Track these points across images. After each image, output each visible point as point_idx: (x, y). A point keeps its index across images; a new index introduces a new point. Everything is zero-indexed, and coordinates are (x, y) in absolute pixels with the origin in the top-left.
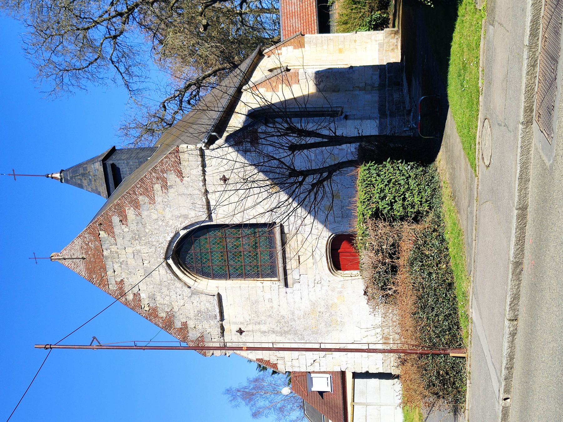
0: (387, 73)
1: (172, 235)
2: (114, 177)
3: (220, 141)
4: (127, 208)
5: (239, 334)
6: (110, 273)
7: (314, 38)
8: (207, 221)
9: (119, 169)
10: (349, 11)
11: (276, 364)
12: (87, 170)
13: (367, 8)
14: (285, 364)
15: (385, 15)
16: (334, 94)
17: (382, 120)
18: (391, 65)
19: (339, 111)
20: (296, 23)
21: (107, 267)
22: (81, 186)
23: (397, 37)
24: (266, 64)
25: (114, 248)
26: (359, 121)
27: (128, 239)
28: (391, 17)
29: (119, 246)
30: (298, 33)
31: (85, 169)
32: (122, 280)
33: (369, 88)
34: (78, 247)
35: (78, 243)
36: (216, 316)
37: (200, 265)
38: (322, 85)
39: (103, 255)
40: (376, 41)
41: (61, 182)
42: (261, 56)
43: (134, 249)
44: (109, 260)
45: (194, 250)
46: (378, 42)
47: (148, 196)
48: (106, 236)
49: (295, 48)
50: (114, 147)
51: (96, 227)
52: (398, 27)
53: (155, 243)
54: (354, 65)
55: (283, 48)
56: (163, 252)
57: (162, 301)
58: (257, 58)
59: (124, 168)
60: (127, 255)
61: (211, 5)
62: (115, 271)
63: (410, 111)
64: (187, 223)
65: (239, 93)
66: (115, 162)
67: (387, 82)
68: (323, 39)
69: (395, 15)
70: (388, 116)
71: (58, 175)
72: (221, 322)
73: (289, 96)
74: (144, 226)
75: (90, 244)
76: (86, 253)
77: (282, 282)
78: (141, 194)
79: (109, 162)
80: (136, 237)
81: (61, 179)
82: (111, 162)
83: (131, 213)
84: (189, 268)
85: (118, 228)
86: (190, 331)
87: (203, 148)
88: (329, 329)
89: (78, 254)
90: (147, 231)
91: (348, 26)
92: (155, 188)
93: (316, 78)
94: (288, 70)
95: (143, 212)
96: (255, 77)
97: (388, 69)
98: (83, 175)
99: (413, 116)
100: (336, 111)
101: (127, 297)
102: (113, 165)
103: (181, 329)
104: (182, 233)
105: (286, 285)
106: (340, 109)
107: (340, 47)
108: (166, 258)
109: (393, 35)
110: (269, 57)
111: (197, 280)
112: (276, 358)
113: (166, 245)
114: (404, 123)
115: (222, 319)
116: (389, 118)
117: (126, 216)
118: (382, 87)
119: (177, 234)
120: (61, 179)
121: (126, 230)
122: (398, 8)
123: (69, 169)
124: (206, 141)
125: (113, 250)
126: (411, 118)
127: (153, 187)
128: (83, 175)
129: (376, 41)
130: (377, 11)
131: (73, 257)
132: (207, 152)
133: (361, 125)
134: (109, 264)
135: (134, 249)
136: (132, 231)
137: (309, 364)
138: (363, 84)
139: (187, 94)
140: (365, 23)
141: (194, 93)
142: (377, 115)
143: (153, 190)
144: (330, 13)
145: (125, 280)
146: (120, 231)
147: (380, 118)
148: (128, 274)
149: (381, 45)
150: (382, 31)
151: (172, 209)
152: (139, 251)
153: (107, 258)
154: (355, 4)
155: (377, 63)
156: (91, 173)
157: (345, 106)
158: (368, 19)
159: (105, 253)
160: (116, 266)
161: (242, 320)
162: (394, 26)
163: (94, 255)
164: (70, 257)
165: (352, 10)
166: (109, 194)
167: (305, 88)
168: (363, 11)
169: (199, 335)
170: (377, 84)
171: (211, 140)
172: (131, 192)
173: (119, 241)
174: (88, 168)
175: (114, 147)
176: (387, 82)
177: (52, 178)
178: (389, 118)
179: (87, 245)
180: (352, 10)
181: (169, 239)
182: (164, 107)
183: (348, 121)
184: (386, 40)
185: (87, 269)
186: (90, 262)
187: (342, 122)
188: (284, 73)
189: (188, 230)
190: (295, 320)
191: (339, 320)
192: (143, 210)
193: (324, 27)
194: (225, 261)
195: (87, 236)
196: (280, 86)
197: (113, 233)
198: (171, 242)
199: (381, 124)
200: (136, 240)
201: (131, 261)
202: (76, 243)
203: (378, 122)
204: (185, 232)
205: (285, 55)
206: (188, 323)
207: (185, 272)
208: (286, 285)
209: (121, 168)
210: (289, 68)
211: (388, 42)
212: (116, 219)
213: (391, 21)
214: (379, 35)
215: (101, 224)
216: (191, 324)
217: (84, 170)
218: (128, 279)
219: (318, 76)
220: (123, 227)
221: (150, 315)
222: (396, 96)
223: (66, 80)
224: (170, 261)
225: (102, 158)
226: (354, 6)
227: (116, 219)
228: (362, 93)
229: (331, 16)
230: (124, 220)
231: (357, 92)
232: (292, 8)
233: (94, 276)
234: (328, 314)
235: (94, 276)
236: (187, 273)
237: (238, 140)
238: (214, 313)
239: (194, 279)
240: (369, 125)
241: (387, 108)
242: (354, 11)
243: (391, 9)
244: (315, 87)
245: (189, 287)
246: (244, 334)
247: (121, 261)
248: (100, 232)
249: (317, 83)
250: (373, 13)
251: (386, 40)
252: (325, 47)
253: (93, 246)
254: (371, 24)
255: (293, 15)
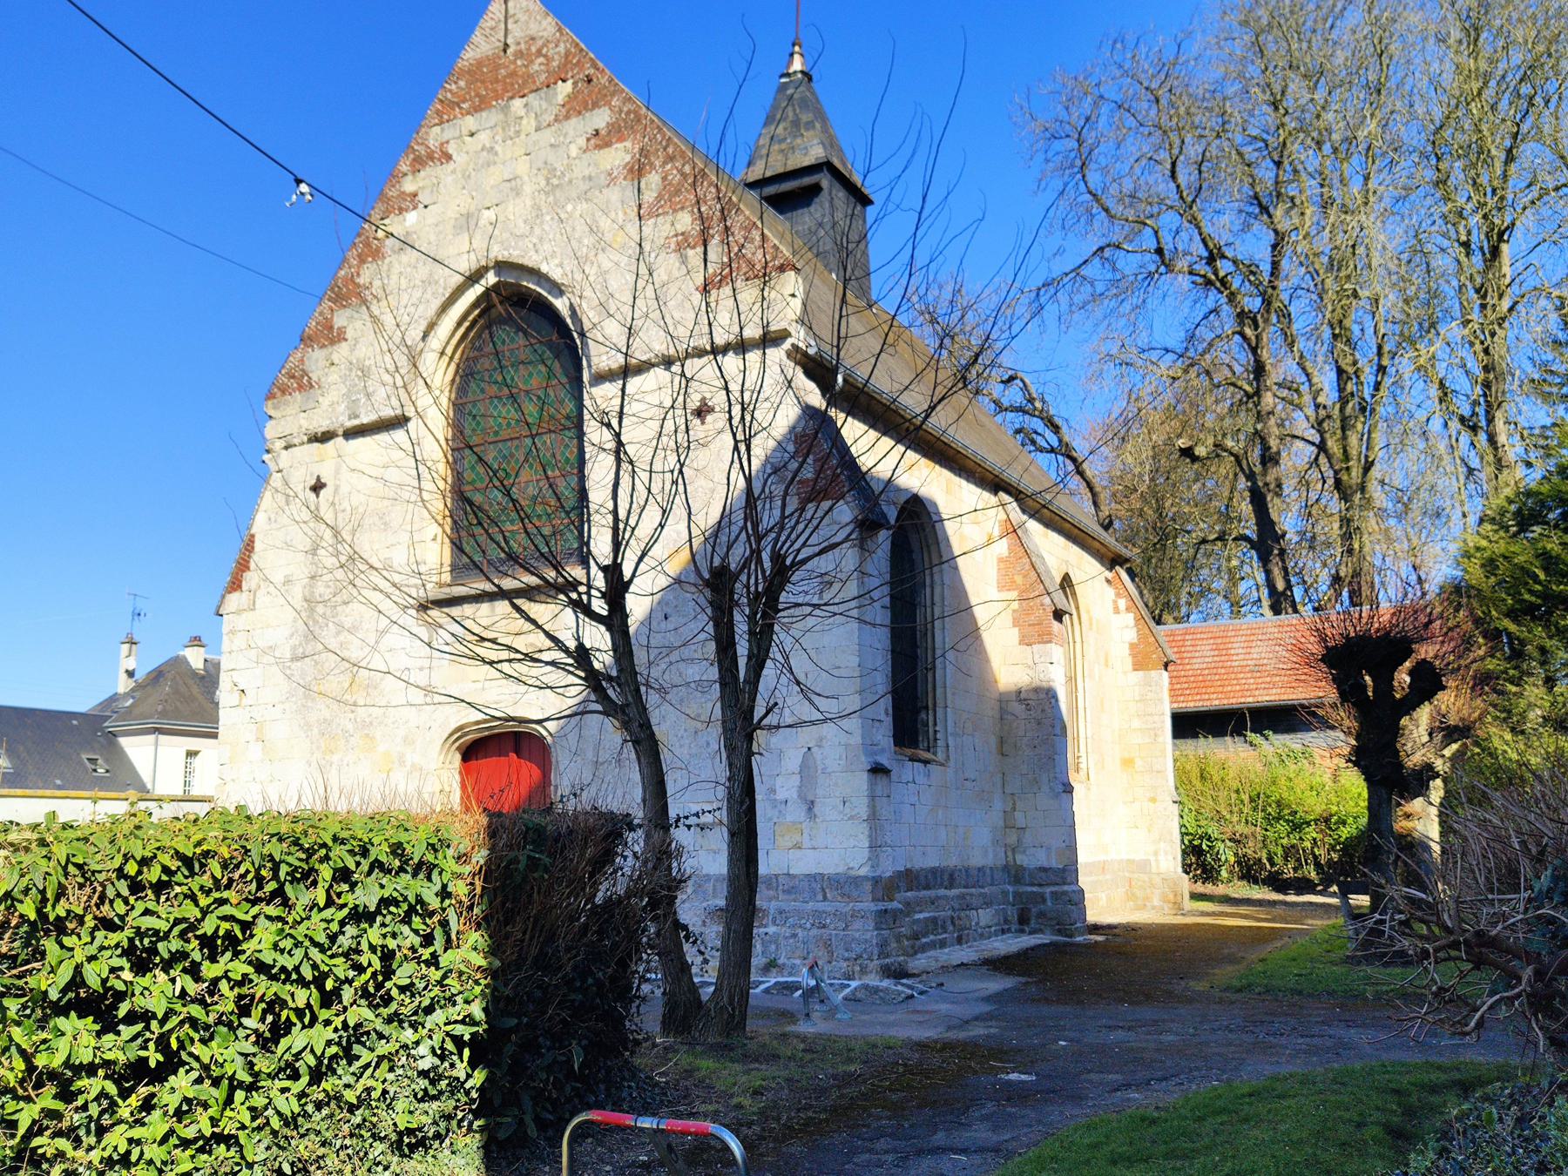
0: (1056, 888)
1: (556, 274)
2: (788, 194)
3: (816, 398)
4: (628, 144)
5: (313, 482)
6: (470, 122)
7: (1158, 699)
8: (590, 366)
9: (809, 205)
10: (1235, 785)
11: (240, 587)
12: (807, 129)
13: (1241, 829)
14: (239, 612)
15: (1224, 874)
16: (993, 740)
17: (868, 886)
18: (1077, 900)
19: (935, 754)
20: (1202, 656)
21: (484, 114)
22: (769, 120)
23: (1167, 908)
24: (1085, 567)
25: (529, 124)
26: (863, 810)
27: (551, 159)
28: (1221, 889)
29: (535, 136)
30: (1169, 652)
31: (810, 125)
32: (449, 157)
33: (1012, 839)
34: (534, 29)
35: (546, 26)
36: (357, 417)
37: (487, 366)
38: (1018, 708)
39: (512, 98)
40: (1156, 853)
41: (783, 76)
42: (1113, 561)
43: (526, 178)
44: (501, 116)
45: (513, 342)
46: (1152, 858)
47: (659, 197)
48: (560, 99)
49: (1132, 646)
50: (870, 202)
51: (581, 70)
52: (1192, 913)
53: (537, 231)
54: (1078, 794)
55: (1131, 616)
56: (515, 255)
57: (396, 269)
58: (1103, 550)
59: (807, 217)
60: (515, 160)
61: (1242, 469)
62: (472, 135)
63: (899, 974)
64: (589, 315)
65: (995, 484)
66: (825, 193)
67: (1029, 889)
68: (1156, 718)
69: (1227, 900)
70: (881, 906)
71: (797, 65)
72: (340, 432)
73: (981, 614)
74: (584, 196)
75: (541, 60)
76: (519, 54)
77: (434, 593)
78: (664, 179)
79: (825, 180)
80: (553, 182)
81: (788, 75)
82: (825, 183)
83: (619, 155)
84: (479, 335)
85: (579, 128)
86: (325, 352)
87: (789, 341)
88: (316, 731)
89: (516, 32)
90: (569, 207)
91: (1192, 785)
92: (680, 215)
93: (1037, 690)
94: (1058, 615)
95: (617, 189)
96: (1046, 536)
97: (1065, 893)
98: (796, 123)
99: (876, 990)
100: (935, 746)
101: (410, 177)
102: (816, 189)
103: (331, 327)
104: (561, 304)
105: (423, 607)
106: (940, 756)
107: (1139, 763)
108: (501, 266)
109: (1171, 896)
110: (1108, 581)
111: (446, 359)
112: (253, 587)
113: (530, 260)
114: (859, 957)
115: (350, 434)
116: (873, 907)
117: (608, 144)
118: (1016, 874)
119: (558, 289)
120: (788, 75)
121: (574, 151)
122: (1243, 910)
123: (813, 93)
124: (811, 351)
125: (524, 122)
126: (873, 980)
127: (682, 208)
128: (796, 123)
129: (1156, 853)
130: (1236, 854)
131: (510, 21)
132: (776, 355)
133: (851, 818)
134: (490, 117)
135: (526, 178)
136: (569, 167)
137: (236, 677)
138: (1021, 822)
139: (1037, 424)
140: (1203, 823)
141: (1039, 439)
142: (888, 869)
143: (675, 211)
144: (1228, 738)
145: (451, 165)
146: (571, 133)
147: (876, 881)
148: (464, 172)
149: (1143, 866)
150: (1180, 870)
151: (620, 259)
152: (517, 192)
153: (505, 110)
154: (1252, 800)
155: (1083, 857)
156: (799, 141)
157: (950, 771)
158: (1213, 830)
159: (517, 103)
160: (484, 138)
161: (344, 489)
162: (1195, 896)
163: (513, 74)
164: (511, 12)
165: (1237, 792)
166: (752, 185)
167: (1008, 658)
168: (1235, 819)
169: (314, 377)
170: (1022, 859)
171: (818, 369)
172: (670, 150)
173: (548, 136)
174: (811, 133)
175: (870, 202)
176: (1029, 889)
177: (792, 55)
178: (873, 907)
179: (539, 53)
180: (1237, 792)
181: (544, 269)
182: (1012, 379)
183: (865, 775)
184: (1157, 880)
185: (480, 63)
186: (497, 67)
187: (863, 758)
188: (1057, 608)
189: (569, 321)
190: (338, 633)
191: (335, 758)
192: (624, 189)
193: (1187, 725)
194: (496, 433)
195: (562, 48)
196: (1014, 595)
197: (567, 117)
198: (534, 273)
199: (856, 881)
200: (548, 180)
201: (495, 175)
202: (544, 23)
203: (863, 872)
204: (565, 312)
205: (1106, 605)
206: (344, 344)
207: (467, 324)
208: (423, 607)
209: (812, 209)
210: (1066, 618)
211: (1152, 886)
212: (601, 118)
213: (1209, 888)
214: (1170, 860)
215: (589, 81)
216: (341, 352)
217: (808, 123)
218: (454, 172)
219: (1042, 696)
220: (582, 142)
221: (367, 244)
222: (985, 917)
223: (1058, 145)
224: (491, 278)
225: (836, 162)
226: (1246, 798)
227: (601, 118)
228: (996, 817)
229: (1219, 740)
230: (600, 140)
231: (998, 805)
232: (1237, 648)
233: (462, 83)
234: (350, 726)
235: (462, 83)
236: (462, 330)
237: (815, 434)
238: (363, 411)
239: (449, 351)
240: (852, 842)
241: (942, 892)
242: (1234, 796)
243: (1241, 890)
244: (1013, 688)
245: (424, 338)
246: (313, 495)
247: (497, 148)
248: (570, 82)
249: (1023, 696)
250: (1229, 844)
251: (1157, 880)
252: (1136, 723)
253: (536, 67)
254: (1201, 838)
255: (1222, 649)
